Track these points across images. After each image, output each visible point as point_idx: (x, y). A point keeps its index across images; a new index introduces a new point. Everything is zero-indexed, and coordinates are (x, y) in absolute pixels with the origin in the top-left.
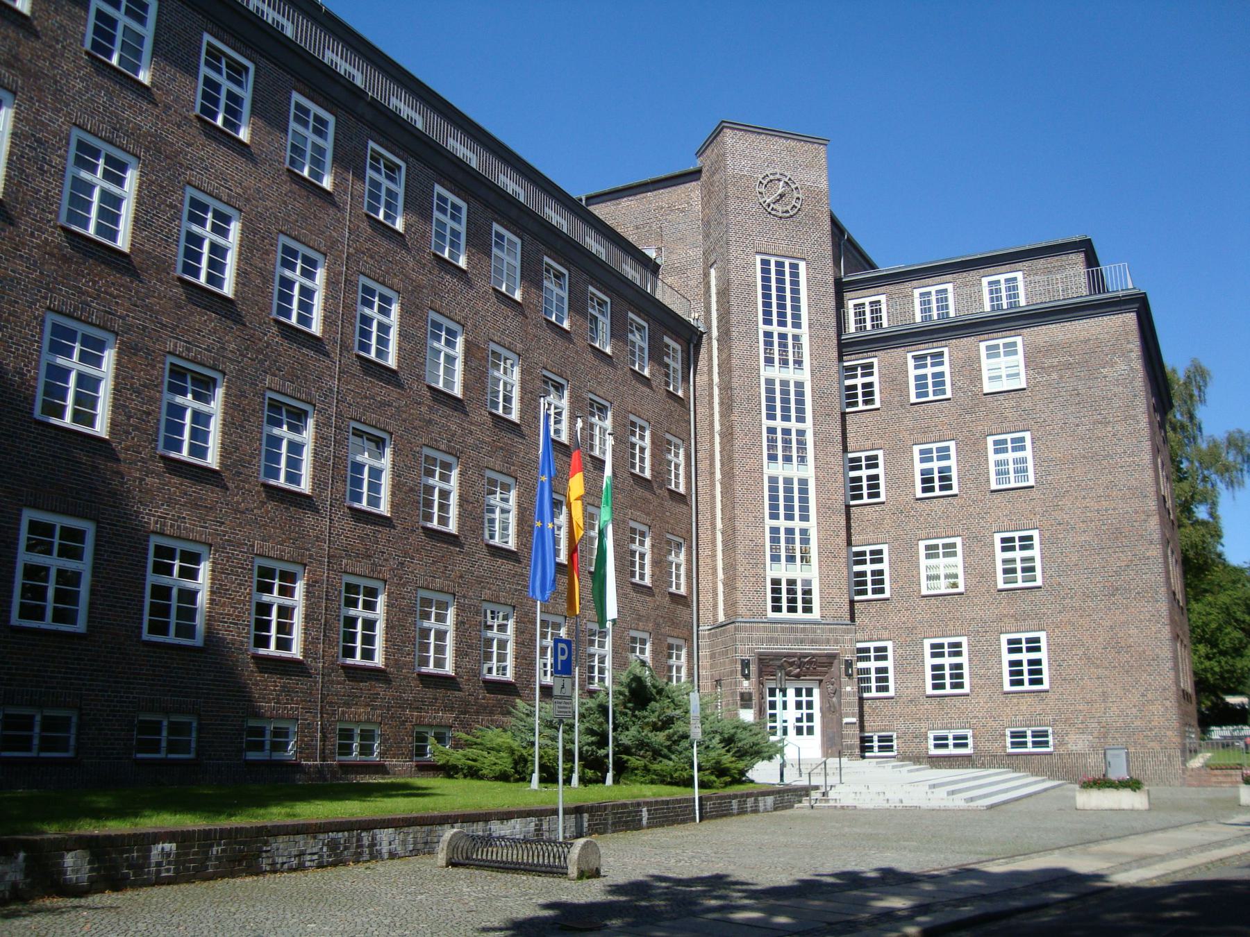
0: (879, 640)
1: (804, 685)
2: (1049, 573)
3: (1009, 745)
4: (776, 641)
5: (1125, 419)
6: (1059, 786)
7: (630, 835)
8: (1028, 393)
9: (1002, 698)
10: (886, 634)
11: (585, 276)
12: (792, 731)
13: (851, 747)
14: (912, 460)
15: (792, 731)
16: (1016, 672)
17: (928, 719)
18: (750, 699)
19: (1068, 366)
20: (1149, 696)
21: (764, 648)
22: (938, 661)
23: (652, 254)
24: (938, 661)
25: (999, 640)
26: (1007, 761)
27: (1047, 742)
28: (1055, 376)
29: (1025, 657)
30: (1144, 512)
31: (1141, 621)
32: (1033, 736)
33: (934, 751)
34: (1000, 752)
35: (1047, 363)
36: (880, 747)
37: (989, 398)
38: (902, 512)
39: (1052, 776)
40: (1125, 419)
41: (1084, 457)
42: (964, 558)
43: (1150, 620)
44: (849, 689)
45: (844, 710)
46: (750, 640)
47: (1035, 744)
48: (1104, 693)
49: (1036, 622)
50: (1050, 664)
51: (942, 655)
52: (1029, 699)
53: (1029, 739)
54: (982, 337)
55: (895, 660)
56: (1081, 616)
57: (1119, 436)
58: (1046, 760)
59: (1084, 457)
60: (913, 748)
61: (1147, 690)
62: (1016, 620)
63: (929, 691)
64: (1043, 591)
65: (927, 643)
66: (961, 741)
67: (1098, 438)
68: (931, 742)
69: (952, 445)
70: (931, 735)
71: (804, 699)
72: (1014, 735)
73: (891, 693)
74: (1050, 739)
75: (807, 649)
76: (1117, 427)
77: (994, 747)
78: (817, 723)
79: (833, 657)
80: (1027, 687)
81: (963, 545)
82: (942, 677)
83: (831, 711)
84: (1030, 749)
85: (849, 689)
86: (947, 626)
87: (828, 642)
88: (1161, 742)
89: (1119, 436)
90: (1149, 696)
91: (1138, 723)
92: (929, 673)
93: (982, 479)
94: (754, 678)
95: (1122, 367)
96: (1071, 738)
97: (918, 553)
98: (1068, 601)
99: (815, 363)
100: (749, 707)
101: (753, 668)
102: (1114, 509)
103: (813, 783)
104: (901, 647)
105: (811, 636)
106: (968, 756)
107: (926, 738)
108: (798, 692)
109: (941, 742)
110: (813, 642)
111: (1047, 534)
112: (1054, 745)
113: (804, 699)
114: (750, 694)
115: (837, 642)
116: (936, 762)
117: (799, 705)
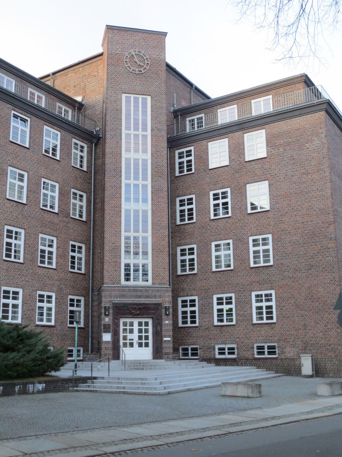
0: (191, 295)
1: (143, 320)
2: (277, 258)
3: (255, 353)
4: (140, 297)
5: (318, 171)
6: (279, 376)
7: (10, 398)
8: (267, 160)
9: (252, 327)
10: (195, 293)
11: (9, 106)
12: (136, 345)
13: (167, 354)
14: (209, 199)
15: (136, 345)
16: (220, 315)
17: (214, 339)
18: (109, 328)
19: (289, 144)
20: (329, 326)
21: (117, 300)
22: (259, 304)
23: (79, 99)
24: (259, 304)
25: (251, 295)
26: (254, 362)
27: (275, 352)
28: (281, 150)
29: (264, 304)
30: (327, 222)
31: (325, 284)
32: (268, 349)
33: (218, 356)
34: (251, 357)
35: (278, 142)
36: (268, 352)
37: (248, 164)
38: (203, 227)
39: (277, 372)
40: (318, 171)
41: (296, 193)
42: (233, 251)
43: (329, 283)
44: (167, 322)
45: (164, 333)
46: (110, 296)
47: (269, 353)
48: (305, 324)
49: (270, 285)
50: (277, 308)
51: (261, 301)
52: (266, 328)
53: (266, 350)
54: (245, 131)
55: (199, 307)
56: (293, 281)
57: (314, 181)
58: (274, 362)
59: (296, 193)
60: (208, 355)
61: (328, 323)
62: (260, 284)
63: (216, 323)
64: (273, 268)
65: (215, 297)
66: (231, 351)
67: (304, 182)
68: (217, 351)
69: (228, 190)
70: (217, 347)
71: (143, 327)
72: (258, 348)
73: (197, 324)
74: (277, 350)
75: (143, 300)
76: (314, 176)
77: (248, 354)
78: (150, 341)
79: (159, 305)
80: (265, 321)
81: (233, 244)
82: (267, 313)
83: (158, 335)
84: (266, 356)
85: (167, 322)
86: (224, 288)
87: (155, 297)
88: (335, 352)
89: (314, 181)
90: (329, 326)
91: (323, 342)
92: (215, 313)
93: (243, 208)
94: (111, 317)
95: (317, 142)
96: (288, 349)
97: (211, 249)
98: (286, 273)
99: (154, 149)
100: (109, 332)
101: (111, 311)
102: (312, 221)
103: (94, 375)
104: (202, 299)
105: (146, 294)
106: (234, 360)
107: (214, 349)
108: (140, 324)
109: (222, 351)
110: (147, 297)
111: (276, 236)
112: (279, 354)
113: (143, 327)
114: (109, 325)
115: (160, 297)
116: (218, 362)
117: (140, 331)
